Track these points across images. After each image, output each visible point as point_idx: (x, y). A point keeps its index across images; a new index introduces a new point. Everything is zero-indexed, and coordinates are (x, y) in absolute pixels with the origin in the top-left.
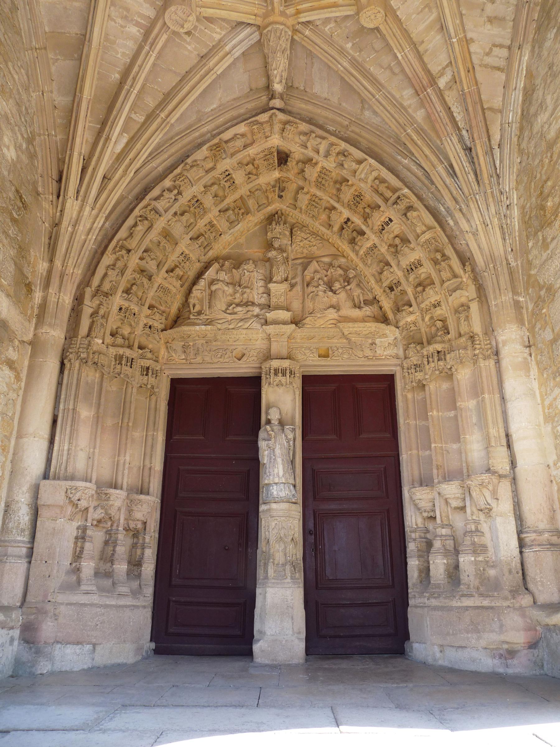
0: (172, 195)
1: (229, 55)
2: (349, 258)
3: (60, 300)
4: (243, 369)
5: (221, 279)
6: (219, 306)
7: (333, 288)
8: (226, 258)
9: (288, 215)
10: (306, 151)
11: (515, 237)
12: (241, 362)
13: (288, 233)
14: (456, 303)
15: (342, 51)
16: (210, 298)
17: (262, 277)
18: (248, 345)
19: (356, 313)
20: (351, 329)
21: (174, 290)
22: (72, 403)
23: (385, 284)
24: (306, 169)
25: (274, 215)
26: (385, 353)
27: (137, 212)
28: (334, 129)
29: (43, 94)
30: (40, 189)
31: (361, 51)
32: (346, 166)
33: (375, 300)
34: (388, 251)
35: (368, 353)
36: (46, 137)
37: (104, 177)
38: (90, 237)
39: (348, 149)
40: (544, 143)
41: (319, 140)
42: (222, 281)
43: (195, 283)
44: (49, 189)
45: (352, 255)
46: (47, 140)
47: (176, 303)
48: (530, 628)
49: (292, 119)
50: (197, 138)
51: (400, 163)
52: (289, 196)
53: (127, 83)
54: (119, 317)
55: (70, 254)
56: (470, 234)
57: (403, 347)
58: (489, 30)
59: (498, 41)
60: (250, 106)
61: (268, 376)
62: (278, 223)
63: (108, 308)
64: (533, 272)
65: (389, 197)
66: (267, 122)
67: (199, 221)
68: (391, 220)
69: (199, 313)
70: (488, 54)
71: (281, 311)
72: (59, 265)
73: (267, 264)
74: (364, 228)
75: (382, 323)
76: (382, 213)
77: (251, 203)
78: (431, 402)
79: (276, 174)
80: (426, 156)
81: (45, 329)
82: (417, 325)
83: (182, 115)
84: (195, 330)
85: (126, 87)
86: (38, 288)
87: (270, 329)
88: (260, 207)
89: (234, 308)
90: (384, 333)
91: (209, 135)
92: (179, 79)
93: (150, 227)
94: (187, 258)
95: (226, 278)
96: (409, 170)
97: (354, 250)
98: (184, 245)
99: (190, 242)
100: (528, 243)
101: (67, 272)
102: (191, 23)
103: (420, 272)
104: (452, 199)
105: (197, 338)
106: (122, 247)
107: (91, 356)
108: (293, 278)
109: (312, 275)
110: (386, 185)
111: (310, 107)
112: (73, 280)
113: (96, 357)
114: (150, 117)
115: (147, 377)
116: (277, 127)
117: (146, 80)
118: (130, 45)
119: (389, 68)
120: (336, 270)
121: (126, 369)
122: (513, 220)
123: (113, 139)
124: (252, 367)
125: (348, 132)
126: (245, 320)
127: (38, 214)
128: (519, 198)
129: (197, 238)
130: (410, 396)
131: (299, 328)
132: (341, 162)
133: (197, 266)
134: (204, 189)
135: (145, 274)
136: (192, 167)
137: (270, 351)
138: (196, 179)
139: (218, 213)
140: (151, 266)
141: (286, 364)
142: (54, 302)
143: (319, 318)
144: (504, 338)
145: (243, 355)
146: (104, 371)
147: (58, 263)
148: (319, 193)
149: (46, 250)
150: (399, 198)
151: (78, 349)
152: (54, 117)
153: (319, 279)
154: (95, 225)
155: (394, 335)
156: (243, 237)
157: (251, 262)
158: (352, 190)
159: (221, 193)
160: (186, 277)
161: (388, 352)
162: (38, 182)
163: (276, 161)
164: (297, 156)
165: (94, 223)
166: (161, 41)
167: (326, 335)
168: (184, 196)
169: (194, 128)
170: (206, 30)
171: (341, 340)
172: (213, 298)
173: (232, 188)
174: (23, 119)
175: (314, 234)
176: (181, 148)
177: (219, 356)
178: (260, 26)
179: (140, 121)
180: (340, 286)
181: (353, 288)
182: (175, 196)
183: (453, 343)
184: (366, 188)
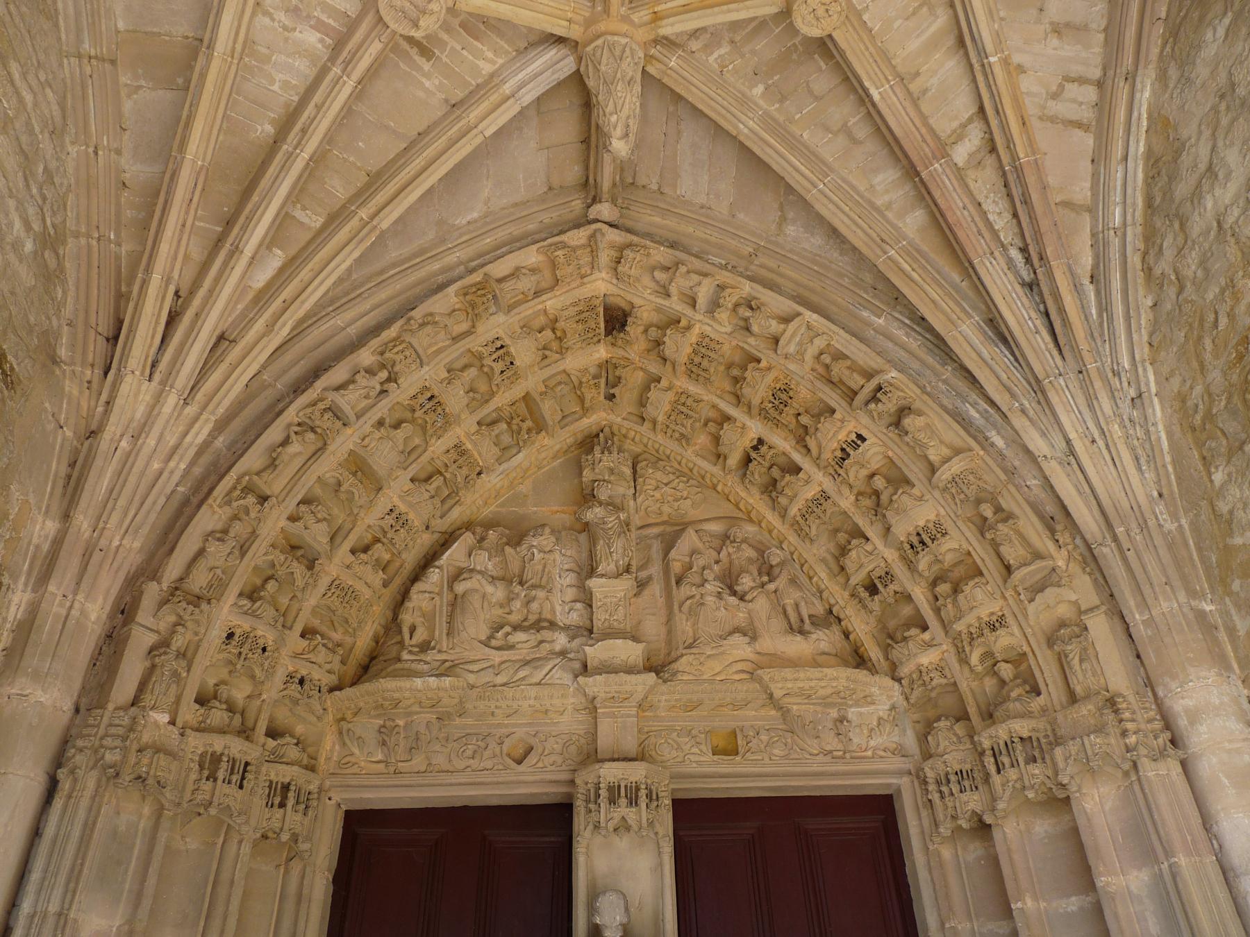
0: (375, 383)
1: (512, 101)
2: (763, 525)
3: (73, 612)
4: (527, 784)
7: (737, 588)
8: (489, 525)
9: (625, 436)
10: (666, 303)
11: (1164, 466)
12: (522, 768)
13: (628, 471)
15: (744, 101)
16: (452, 611)
17: (572, 566)
19: (796, 646)
22: (57, 893)
25: (597, 435)
26: (872, 743)
27: (292, 414)
28: (724, 262)
29: (96, 153)
30: (63, 352)
31: (783, 99)
32: (755, 328)
33: (831, 617)
34: (858, 507)
35: (831, 743)
36: (94, 243)
37: (221, 338)
38: (172, 464)
39: (758, 296)
42: (480, 572)
43: (418, 574)
44: (84, 353)
45: (771, 517)
46: (95, 249)
47: (369, 624)
49: (635, 239)
50: (435, 274)
51: (869, 324)
52: (627, 397)
54: (225, 655)
55: (116, 500)
56: (1054, 463)
57: (914, 728)
58: (1055, 49)
59: (1076, 70)
60: (546, 218)
61: (592, 806)
62: (606, 449)
63: (196, 634)
65: (855, 387)
67: (433, 441)
68: (861, 438)
69: (425, 647)
70: (1055, 96)
71: (619, 642)
72: (85, 525)
73: (583, 537)
74: (797, 457)
75: (857, 667)
77: (548, 408)
79: (602, 352)
80: (933, 302)
82: (947, 672)
83: (400, 220)
84: (412, 688)
85: (285, 147)
86: (23, 579)
87: (595, 685)
89: (508, 634)
90: (867, 693)
91: (462, 268)
93: (322, 449)
94: (401, 521)
95: (490, 567)
96: (889, 337)
98: (396, 493)
99: (411, 485)
100: (1209, 474)
101: (103, 543)
102: (434, 18)
103: (944, 548)
104: (1001, 388)
105: (416, 708)
106: (248, 490)
107: (132, 759)
108: (641, 568)
109: (687, 559)
110: (849, 363)
111: (671, 222)
112: (115, 565)
113: (145, 761)
114: (335, 219)
115: (282, 810)
116: (605, 257)
117: (329, 139)
118: (302, 68)
119: (845, 130)
121: (227, 793)
122: (1152, 429)
123: (249, 250)
124: (551, 782)
125: (753, 267)
126: (533, 664)
127: (47, 405)
128: (1163, 380)
129: (428, 479)
130: (946, 853)
131: (665, 681)
133: (426, 540)
134: (446, 375)
135: (300, 553)
136: (423, 325)
137: (595, 740)
138: (430, 351)
139: (475, 428)
140: (317, 535)
141: (636, 773)
143: (709, 656)
144: (1189, 703)
146: (164, 801)
147: (82, 522)
148: (693, 388)
149: (59, 490)
151: (102, 739)
152: (118, 204)
153: (704, 568)
154: (188, 439)
155: (890, 697)
157: (547, 530)
159: (483, 387)
160: (397, 564)
161: (880, 740)
162: (58, 336)
163: (602, 325)
164: (645, 315)
166: (367, 55)
170: (465, 53)
171: (763, 712)
172: (458, 610)
173: (508, 374)
174: (34, 191)
175: (685, 474)
177: (469, 753)
178: (577, 43)
179: (313, 225)
181: (781, 586)
182: (382, 384)
183: (1060, 717)
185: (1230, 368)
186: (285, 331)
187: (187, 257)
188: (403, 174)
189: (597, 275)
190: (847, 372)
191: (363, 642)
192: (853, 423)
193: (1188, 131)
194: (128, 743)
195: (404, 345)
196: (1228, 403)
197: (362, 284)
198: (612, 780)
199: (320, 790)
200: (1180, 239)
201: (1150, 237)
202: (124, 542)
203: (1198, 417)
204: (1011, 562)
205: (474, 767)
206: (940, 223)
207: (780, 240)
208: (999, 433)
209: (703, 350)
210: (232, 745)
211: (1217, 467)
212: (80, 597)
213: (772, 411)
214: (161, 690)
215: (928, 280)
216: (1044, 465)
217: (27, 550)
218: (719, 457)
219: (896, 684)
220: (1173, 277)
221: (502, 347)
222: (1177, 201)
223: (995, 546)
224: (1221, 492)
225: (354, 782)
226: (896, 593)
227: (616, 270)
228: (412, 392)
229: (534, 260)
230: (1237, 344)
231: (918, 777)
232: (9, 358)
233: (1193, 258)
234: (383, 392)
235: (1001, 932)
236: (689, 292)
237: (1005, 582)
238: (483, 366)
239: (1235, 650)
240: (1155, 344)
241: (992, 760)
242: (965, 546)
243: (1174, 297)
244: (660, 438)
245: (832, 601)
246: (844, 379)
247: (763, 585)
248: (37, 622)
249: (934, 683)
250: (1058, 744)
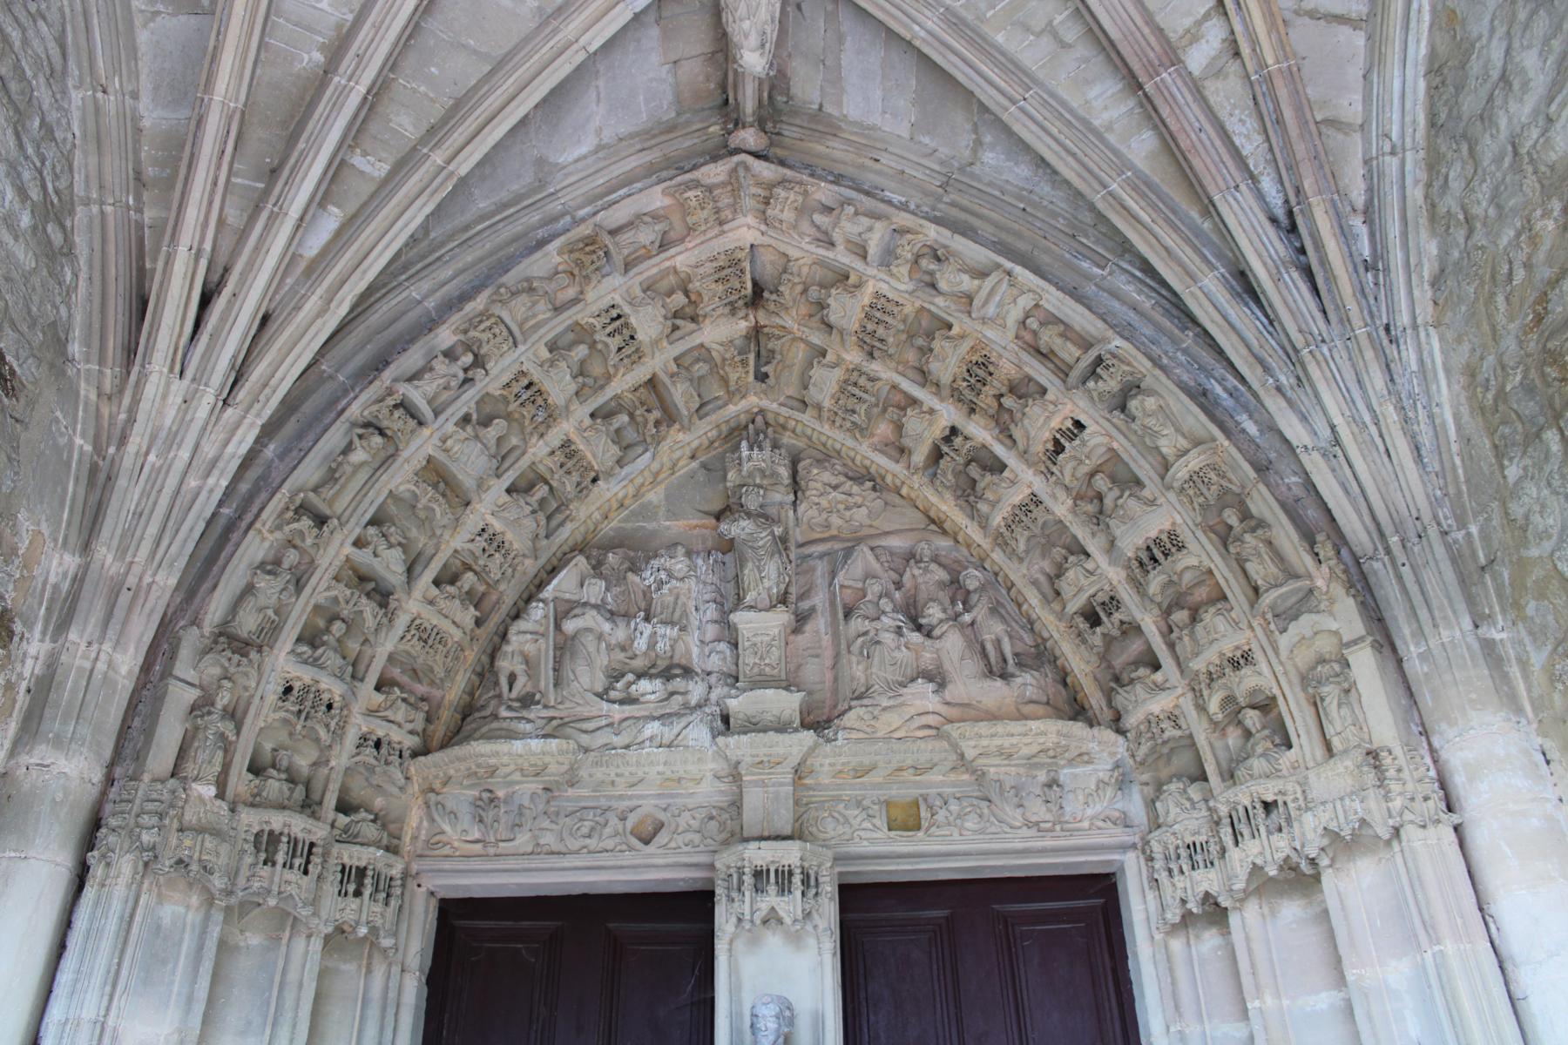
0: (457, 369)
5: (593, 601)
6: (585, 680)
7: (923, 621)
10: (830, 254)
12: (651, 849)
13: (784, 472)
14: (1304, 657)
18: (672, 796)
19: (994, 693)
20: (985, 742)
21: (457, 635)
23: (1072, 607)
24: (830, 301)
25: (746, 427)
26: (1089, 812)
33: (1041, 656)
34: (1075, 513)
38: (211, 481)
40: (1531, 182)
41: (866, 221)
45: (973, 532)
47: (461, 672)
48: (755, 941)
49: (788, 173)
53: (341, 70)
56: (1316, 455)
61: (734, 894)
64: (1534, 552)
65: (1070, 360)
66: (723, 184)
67: (534, 440)
68: (1079, 425)
69: (527, 701)
74: (1000, 450)
75: (1074, 718)
76: (1051, 407)
77: (680, 394)
78: (1253, 965)
80: (1166, 249)
81: (41, 753)
82: (1182, 722)
84: (517, 754)
85: (336, 79)
86: (39, 627)
87: (740, 746)
88: (701, 411)
90: (1084, 749)
92: (487, 68)
93: (393, 456)
94: (495, 543)
96: (1115, 294)
97: (972, 512)
99: (506, 498)
100: (1502, 468)
103: (1179, 567)
104: (1251, 359)
105: (517, 777)
108: (801, 597)
112: (148, 606)
114: (404, 164)
115: (358, 900)
119: (1050, 30)
120: (926, 570)
125: (942, 206)
127: (58, 414)
132: (927, 278)
133: (530, 567)
135: (372, 585)
139: (588, 421)
140: (389, 565)
141: (790, 854)
142: (80, 669)
143: (885, 709)
145: (660, 826)
150: (1099, 360)
154: (230, 449)
156: (661, 489)
157: (681, 550)
158: (966, 346)
160: (494, 598)
161: (1099, 808)
164: (805, 270)
165: (227, 442)
167: (909, 762)
168: (493, 372)
169: (525, 203)
171: (953, 777)
176: (491, 254)
177: (585, 830)
179: (376, 174)
180: (942, 616)
181: (979, 618)
182: (466, 370)
184: (1002, 342)
185: (1526, 334)
186: (344, 310)
187: (221, 222)
188: (486, 104)
189: (741, 220)
190: (1059, 341)
191: (454, 693)
192: (1069, 406)
193: (1479, 28)
194: (167, 821)
195: (493, 320)
196: (1524, 378)
197: (443, 244)
198: (759, 863)
199: (406, 875)
200: (1470, 169)
201: (1434, 163)
202: (157, 578)
203: (1490, 396)
204: (1260, 582)
205: (592, 848)
206: (1171, 147)
207: (976, 169)
208: (1251, 417)
209: (878, 314)
210: (294, 822)
211: (1511, 459)
212: (107, 647)
213: (967, 392)
214: (207, 760)
215: (1160, 221)
216: (1304, 458)
217: (43, 590)
218: (902, 451)
219: (1121, 739)
220: (1461, 217)
221: (619, 317)
222: (1465, 118)
223: (1241, 563)
224: (1515, 492)
225: (447, 865)
226: (1122, 623)
227: (764, 212)
228: (505, 379)
229: (658, 204)
230: (1536, 303)
231: (1144, 852)
232: (8, 358)
233: (1484, 192)
234: (466, 381)
235: (1238, 1035)
236: (856, 239)
237: (1252, 606)
238: (595, 342)
239: (1529, 690)
240: (1441, 302)
241: (1230, 830)
242: (1207, 563)
243: (1462, 241)
244: (826, 428)
245: (1046, 635)
246: (1056, 349)
247: (957, 616)
248: (58, 678)
249: (1166, 735)
250: (1308, 809)
